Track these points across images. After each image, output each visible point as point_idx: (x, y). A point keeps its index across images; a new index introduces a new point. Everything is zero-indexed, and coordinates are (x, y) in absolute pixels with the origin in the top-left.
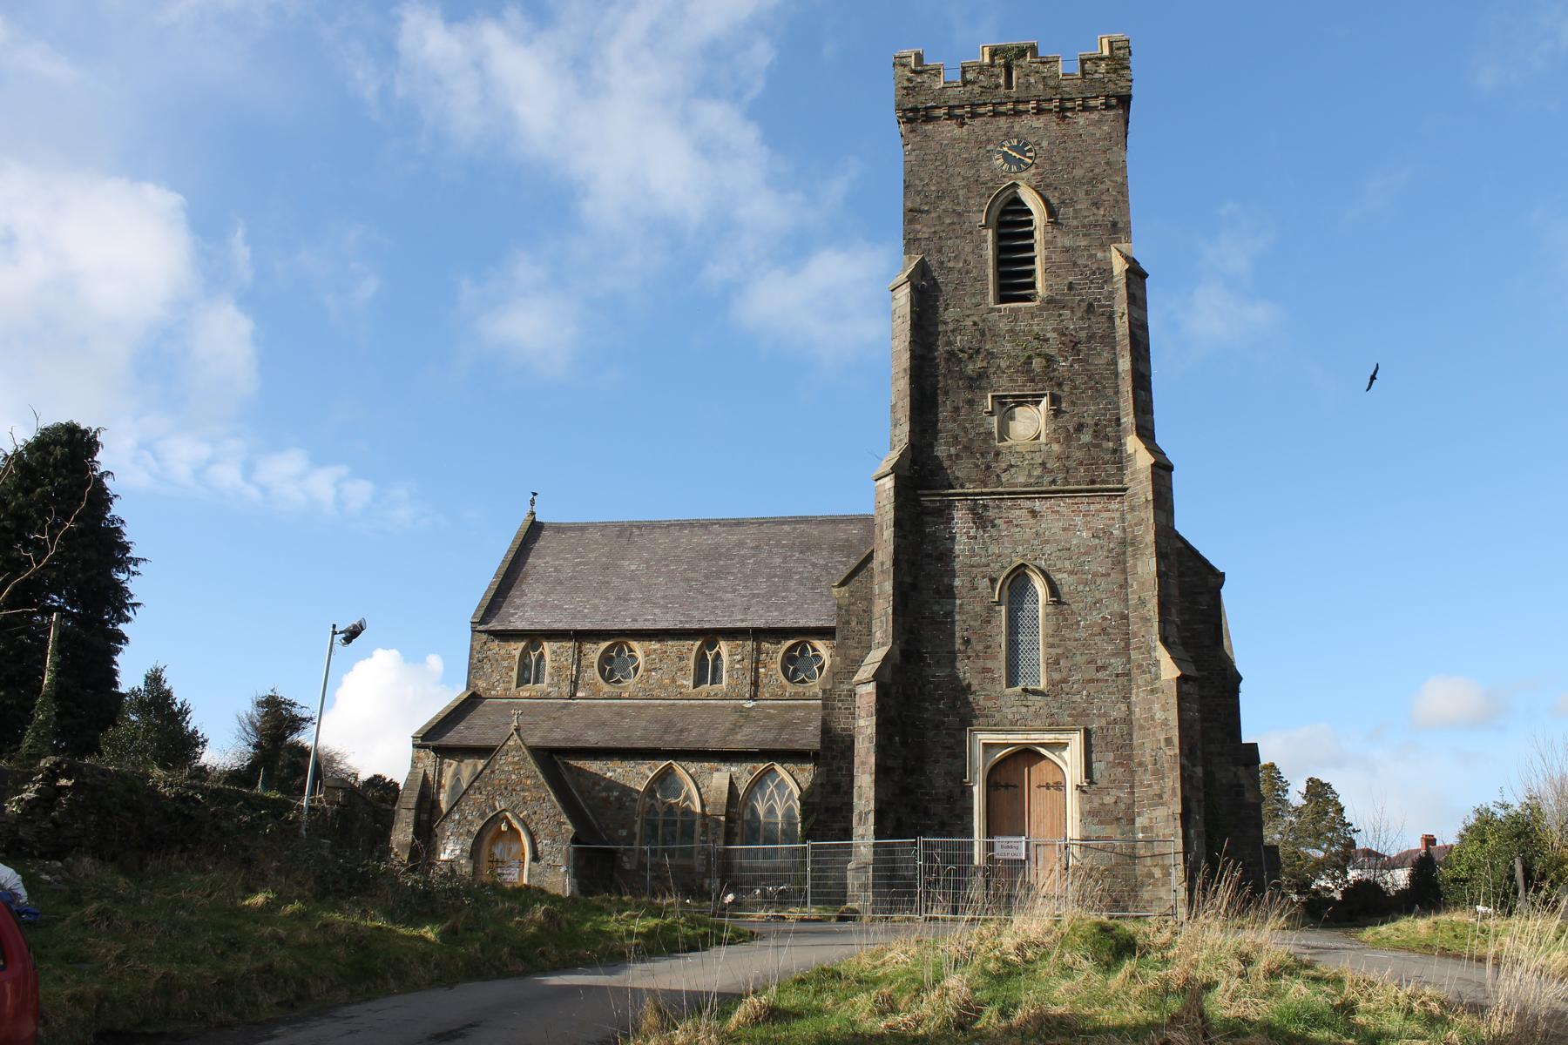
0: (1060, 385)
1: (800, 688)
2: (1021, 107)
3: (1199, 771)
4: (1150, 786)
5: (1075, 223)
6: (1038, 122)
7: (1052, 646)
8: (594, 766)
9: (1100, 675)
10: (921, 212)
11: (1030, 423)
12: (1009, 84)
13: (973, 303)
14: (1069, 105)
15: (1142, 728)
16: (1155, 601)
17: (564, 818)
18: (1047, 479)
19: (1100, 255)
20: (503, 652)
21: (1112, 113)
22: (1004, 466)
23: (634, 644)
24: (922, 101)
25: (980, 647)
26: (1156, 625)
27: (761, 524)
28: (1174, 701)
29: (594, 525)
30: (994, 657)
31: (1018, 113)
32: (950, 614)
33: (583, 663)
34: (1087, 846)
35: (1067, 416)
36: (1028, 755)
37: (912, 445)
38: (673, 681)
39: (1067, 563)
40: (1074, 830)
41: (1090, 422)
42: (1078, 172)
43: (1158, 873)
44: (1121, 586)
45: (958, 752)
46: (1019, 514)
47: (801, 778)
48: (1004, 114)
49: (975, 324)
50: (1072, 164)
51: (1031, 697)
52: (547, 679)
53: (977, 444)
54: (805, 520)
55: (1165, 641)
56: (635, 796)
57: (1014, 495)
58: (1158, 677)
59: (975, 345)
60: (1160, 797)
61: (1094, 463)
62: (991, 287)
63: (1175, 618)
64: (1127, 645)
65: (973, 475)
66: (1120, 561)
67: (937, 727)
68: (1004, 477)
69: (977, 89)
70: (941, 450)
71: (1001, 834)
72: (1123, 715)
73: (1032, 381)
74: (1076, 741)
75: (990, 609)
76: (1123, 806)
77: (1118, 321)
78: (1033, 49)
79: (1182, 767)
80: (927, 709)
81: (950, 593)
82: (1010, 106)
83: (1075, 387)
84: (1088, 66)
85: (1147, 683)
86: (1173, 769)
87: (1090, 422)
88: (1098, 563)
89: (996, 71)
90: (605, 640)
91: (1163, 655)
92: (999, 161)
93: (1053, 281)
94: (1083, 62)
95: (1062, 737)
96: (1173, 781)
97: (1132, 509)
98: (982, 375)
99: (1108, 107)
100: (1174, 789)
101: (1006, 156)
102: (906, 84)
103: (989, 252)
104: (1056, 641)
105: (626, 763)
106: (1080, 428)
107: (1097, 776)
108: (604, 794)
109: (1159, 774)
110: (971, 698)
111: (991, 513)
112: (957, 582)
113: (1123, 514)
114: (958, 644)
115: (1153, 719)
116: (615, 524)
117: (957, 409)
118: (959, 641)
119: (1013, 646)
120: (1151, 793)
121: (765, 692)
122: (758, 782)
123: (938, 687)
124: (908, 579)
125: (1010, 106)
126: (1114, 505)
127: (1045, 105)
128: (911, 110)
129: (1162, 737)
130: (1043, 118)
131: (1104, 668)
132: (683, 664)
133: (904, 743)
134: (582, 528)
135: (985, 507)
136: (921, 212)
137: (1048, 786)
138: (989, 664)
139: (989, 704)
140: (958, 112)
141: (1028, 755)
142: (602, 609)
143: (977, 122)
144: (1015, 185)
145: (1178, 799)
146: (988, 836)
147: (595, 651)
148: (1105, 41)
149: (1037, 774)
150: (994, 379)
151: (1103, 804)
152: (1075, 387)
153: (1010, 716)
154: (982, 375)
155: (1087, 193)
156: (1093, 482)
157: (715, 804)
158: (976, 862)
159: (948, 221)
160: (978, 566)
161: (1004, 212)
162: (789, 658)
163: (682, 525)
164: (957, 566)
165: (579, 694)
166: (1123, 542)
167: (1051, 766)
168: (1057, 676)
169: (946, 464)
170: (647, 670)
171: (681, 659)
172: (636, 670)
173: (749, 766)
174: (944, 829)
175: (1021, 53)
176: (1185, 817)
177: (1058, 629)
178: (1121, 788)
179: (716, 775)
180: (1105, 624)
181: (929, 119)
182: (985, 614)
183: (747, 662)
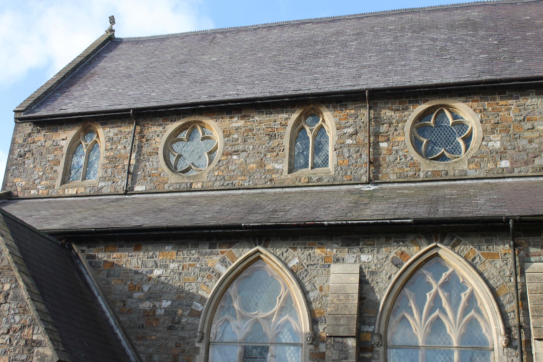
1: (440, 166)
8: (131, 260)
17: (39, 334)
20: (49, 143)
27: (363, 18)
33: (145, 150)
38: (261, 164)
47: (490, 270)
54: (412, 11)
56: (198, 306)
108: (147, 305)
121: (389, 173)
122: (410, 279)
147: (159, 133)
157: (336, 317)
162: (420, 125)
163: (269, 27)
170: (226, 154)
171: (272, 136)
173: (393, 251)
179: (335, 268)
183: (362, 136)
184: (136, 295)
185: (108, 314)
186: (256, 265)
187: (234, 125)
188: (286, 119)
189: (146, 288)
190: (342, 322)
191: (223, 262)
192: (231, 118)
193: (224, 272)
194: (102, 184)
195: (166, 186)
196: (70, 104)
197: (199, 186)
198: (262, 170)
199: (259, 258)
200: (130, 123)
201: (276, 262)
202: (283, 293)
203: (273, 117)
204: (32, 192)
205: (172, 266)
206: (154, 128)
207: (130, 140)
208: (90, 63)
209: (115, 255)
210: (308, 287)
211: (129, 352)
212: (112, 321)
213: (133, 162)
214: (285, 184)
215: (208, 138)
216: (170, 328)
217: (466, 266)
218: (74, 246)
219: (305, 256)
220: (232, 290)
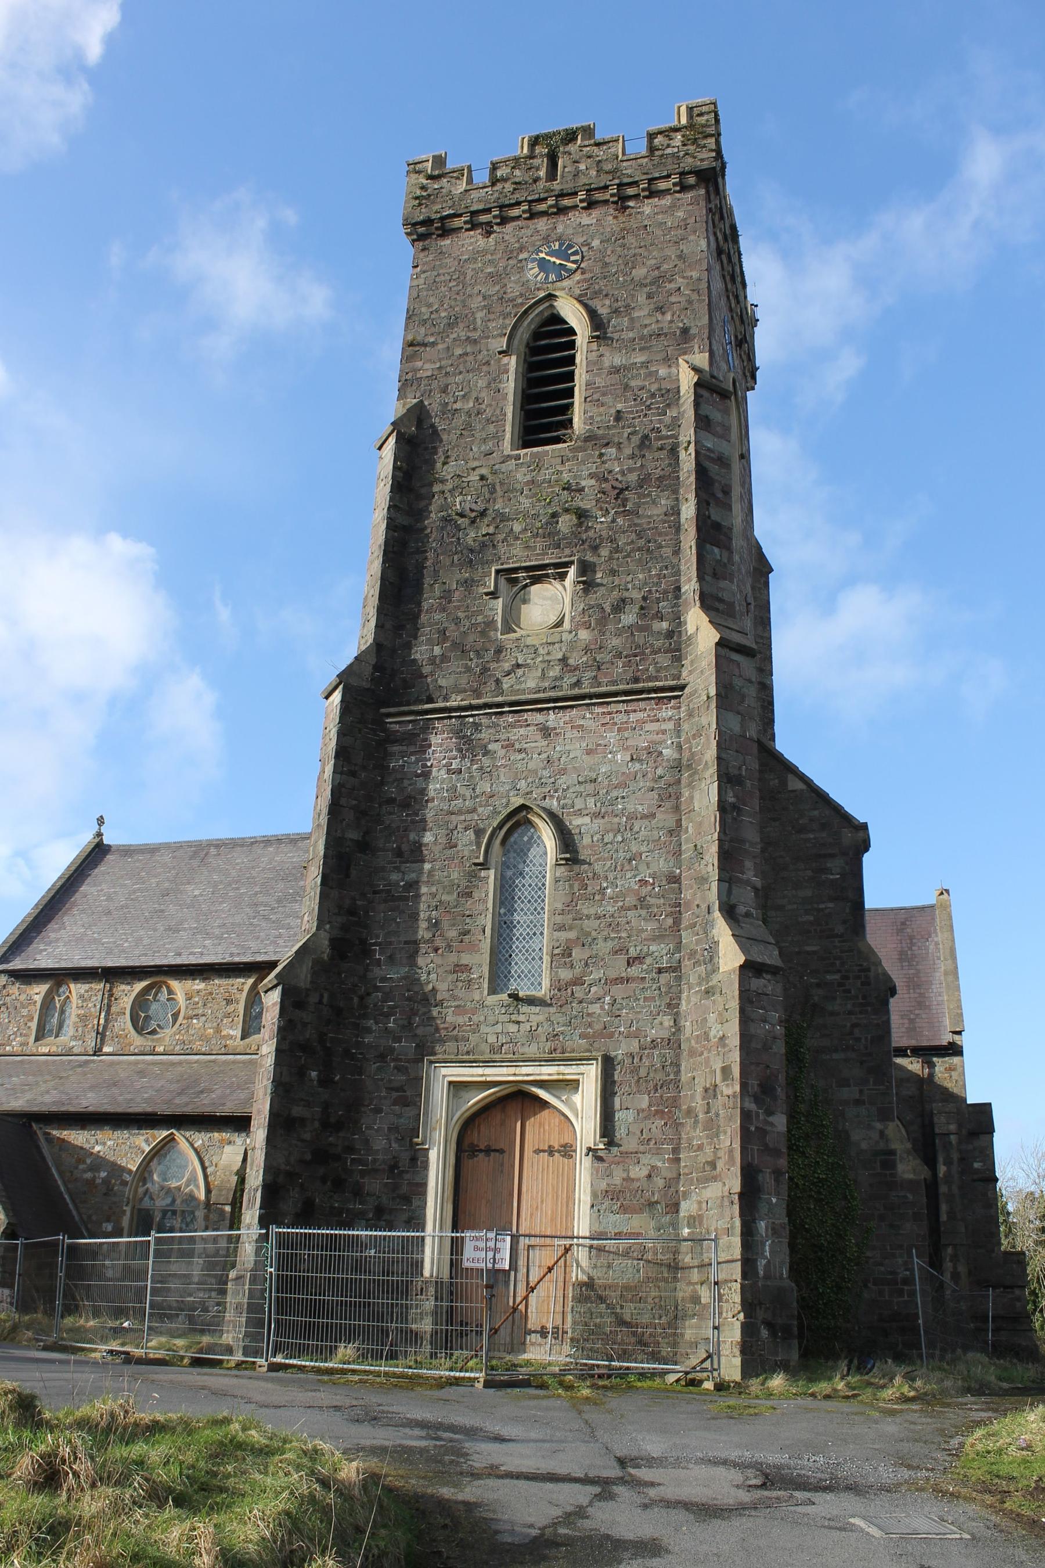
0: (595, 548)
2: (566, 202)
3: (780, 1122)
4: (700, 1148)
5: (631, 335)
6: (587, 219)
7: (561, 928)
8: (78, 1137)
9: (634, 971)
10: (425, 345)
11: (550, 604)
12: (553, 176)
13: (485, 450)
14: (631, 191)
15: (692, 1053)
16: (714, 848)
18: (569, 680)
19: (662, 372)
20: (23, 997)
21: (689, 195)
22: (507, 666)
23: (175, 984)
24: (435, 210)
25: (452, 934)
26: (715, 886)
28: (734, 1004)
29: (167, 846)
30: (473, 948)
31: (562, 211)
32: (413, 885)
33: (113, 1009)
34: (600, 1249)
35: (602, 590)
36: (520, 1100)
37: (378, 645)
38: (218, 1030)
39: (591, 801)
40: (582, 1224)
41: (636, 595)
42: (639, 272)
43: (705, 1295)
44: (671, 832)
45: (410, 1096)
46: (524, 731)
48: (544, 213)
49: (482, 478)
50: (631, 263)
51: (525, 1009)
52: (69, 1030)
53: (471, 638)
55: (729, 912)
56: (128, 1178)
57: (518, 706)
58: (715, 970)
59: (480, 507)
60: (713, 1165)
61: (638, 652)
62: (508, 428)
63: (750, 874)
64: (677, 922)
65: (463, 681)
66: (671, 794)
67: (382, 1057)
68: (507, 683)
69: (509, 187)
70: (421, 652)
71: (473, 1228)
72: (665, 1034)
73: (558, 546)
74: (590, 1075)
75: (472, 876)
76: (660, 1182)
77: (682, 455)
78: (588, 131)
79: (746, 1116)
80: (369, 1030)
81: (416, 853)
82: (551, 202)
83: (617, 550)
84: (658, 140)
85: (701, 980)
86: (730, 1119)
87: (636, 595)
88: (640, 802)
89: (536, 162)
90: (141, 980)
91: (722, 932)
92: (533, 272)
93: (594, 411)
94: (651, 136)
95: (569, 1071)
96: (730, 1139)
97: (690, 715)
98: (488, 543)
99: (684, 188)
100: (731, 1151)
101: (543, 264)
102: (418, 193)
103: (510, 385)
104: (568, 919)
105: (118, 1133)
106: (620, 606)
107: (620, 1132)
108: (88, 1175)
109: (712, 1127)
110: (435, 1012)
111: (485, 735)
112: (428, 838)
113: (678, 723)
114: (423, 931)
115: (706, 1036)
116: (189, 844)
117: (447, 595)
118: (423, 925)
119: (503, 930)
120: (702, 1159)
123: (387, 996)
124: (353, 835)
125: (551, 202)
126: (666, 712)
127: (599, 196)
128: (423, 223)
129: (718, 1066)
130: (596, 213)
131: (639, 959)
132: (230, 1008)
133: (325, 1082)
134: (151, 850)
135: (477, 726)
136: (425, 345)
137: (551, 1152)
138: (466, 959)
139: (460, 1020)
140: (484, 218)
141: (520, 1100)
142: (146, 941)
143: (510, 227)
144: (551, 297)
145: (736, 1170)
146: (455, 1227)
147: (128, 993)
148: (683, 110)
149: (537, 1131)
150: (502, 549)
151: (628, 1179)
152: (617, 550)
153: (492, 1039)
154: (488, 543)
155: (649, 296)
156: (636, 680)
158: (427, 1273)
159: (458, 351)
160: (460, 812)
161: (537, 335)
163: (267, 841)
164: (429, 814)
165: (106, 1049)
166: (678, 766)
167: (556, 1120)
168: (565, 975)
169: (426, 670)
171: (229, 1002)
172: (175, 1016)
174: (381, 1217)
175: (570, 136)
176: (749, 1198)
177: (571, 903)
178: (658, 1152)
179: (228, 1149)
180: (644, 891)
181: (445, 232)
182: (464, 883)
184: (81, 1167)
185: (59, 1182)
186: (172, 1144)
187: (196, 987)
188: (243, 984)
189: (88, 1161)
190: (223, 1192)
191: (147, 1141)
192: (194, 980)
193: (147, 1149)
194: (73, 1043)
195: (132, 1048)
196: (44, 956)
197: (161, 1049)
198: (218, 1035)
199: (174, 1139)
200: (100, 980)
201: (185, 1142)
202: (190, 1168)
203: (231, 981)
204: (8, 1048)
205: (109, 1143)
206: (123, 987)
207: (100, 998)
208: (72, 885)
209: (65, 1132)
210: (207, 1164)
211: (74, 1213)
212: (62, 1189)
213: (102, 1021)
214: (238, 1051)
215: (173, 999)
216: (105, 1194)
217: (528, 1075)
218: (34, 1125)
219: (206, 1139)
220: (154, 1164)
